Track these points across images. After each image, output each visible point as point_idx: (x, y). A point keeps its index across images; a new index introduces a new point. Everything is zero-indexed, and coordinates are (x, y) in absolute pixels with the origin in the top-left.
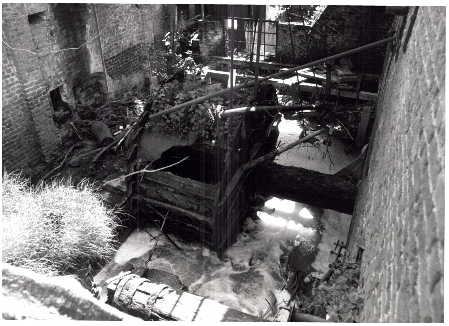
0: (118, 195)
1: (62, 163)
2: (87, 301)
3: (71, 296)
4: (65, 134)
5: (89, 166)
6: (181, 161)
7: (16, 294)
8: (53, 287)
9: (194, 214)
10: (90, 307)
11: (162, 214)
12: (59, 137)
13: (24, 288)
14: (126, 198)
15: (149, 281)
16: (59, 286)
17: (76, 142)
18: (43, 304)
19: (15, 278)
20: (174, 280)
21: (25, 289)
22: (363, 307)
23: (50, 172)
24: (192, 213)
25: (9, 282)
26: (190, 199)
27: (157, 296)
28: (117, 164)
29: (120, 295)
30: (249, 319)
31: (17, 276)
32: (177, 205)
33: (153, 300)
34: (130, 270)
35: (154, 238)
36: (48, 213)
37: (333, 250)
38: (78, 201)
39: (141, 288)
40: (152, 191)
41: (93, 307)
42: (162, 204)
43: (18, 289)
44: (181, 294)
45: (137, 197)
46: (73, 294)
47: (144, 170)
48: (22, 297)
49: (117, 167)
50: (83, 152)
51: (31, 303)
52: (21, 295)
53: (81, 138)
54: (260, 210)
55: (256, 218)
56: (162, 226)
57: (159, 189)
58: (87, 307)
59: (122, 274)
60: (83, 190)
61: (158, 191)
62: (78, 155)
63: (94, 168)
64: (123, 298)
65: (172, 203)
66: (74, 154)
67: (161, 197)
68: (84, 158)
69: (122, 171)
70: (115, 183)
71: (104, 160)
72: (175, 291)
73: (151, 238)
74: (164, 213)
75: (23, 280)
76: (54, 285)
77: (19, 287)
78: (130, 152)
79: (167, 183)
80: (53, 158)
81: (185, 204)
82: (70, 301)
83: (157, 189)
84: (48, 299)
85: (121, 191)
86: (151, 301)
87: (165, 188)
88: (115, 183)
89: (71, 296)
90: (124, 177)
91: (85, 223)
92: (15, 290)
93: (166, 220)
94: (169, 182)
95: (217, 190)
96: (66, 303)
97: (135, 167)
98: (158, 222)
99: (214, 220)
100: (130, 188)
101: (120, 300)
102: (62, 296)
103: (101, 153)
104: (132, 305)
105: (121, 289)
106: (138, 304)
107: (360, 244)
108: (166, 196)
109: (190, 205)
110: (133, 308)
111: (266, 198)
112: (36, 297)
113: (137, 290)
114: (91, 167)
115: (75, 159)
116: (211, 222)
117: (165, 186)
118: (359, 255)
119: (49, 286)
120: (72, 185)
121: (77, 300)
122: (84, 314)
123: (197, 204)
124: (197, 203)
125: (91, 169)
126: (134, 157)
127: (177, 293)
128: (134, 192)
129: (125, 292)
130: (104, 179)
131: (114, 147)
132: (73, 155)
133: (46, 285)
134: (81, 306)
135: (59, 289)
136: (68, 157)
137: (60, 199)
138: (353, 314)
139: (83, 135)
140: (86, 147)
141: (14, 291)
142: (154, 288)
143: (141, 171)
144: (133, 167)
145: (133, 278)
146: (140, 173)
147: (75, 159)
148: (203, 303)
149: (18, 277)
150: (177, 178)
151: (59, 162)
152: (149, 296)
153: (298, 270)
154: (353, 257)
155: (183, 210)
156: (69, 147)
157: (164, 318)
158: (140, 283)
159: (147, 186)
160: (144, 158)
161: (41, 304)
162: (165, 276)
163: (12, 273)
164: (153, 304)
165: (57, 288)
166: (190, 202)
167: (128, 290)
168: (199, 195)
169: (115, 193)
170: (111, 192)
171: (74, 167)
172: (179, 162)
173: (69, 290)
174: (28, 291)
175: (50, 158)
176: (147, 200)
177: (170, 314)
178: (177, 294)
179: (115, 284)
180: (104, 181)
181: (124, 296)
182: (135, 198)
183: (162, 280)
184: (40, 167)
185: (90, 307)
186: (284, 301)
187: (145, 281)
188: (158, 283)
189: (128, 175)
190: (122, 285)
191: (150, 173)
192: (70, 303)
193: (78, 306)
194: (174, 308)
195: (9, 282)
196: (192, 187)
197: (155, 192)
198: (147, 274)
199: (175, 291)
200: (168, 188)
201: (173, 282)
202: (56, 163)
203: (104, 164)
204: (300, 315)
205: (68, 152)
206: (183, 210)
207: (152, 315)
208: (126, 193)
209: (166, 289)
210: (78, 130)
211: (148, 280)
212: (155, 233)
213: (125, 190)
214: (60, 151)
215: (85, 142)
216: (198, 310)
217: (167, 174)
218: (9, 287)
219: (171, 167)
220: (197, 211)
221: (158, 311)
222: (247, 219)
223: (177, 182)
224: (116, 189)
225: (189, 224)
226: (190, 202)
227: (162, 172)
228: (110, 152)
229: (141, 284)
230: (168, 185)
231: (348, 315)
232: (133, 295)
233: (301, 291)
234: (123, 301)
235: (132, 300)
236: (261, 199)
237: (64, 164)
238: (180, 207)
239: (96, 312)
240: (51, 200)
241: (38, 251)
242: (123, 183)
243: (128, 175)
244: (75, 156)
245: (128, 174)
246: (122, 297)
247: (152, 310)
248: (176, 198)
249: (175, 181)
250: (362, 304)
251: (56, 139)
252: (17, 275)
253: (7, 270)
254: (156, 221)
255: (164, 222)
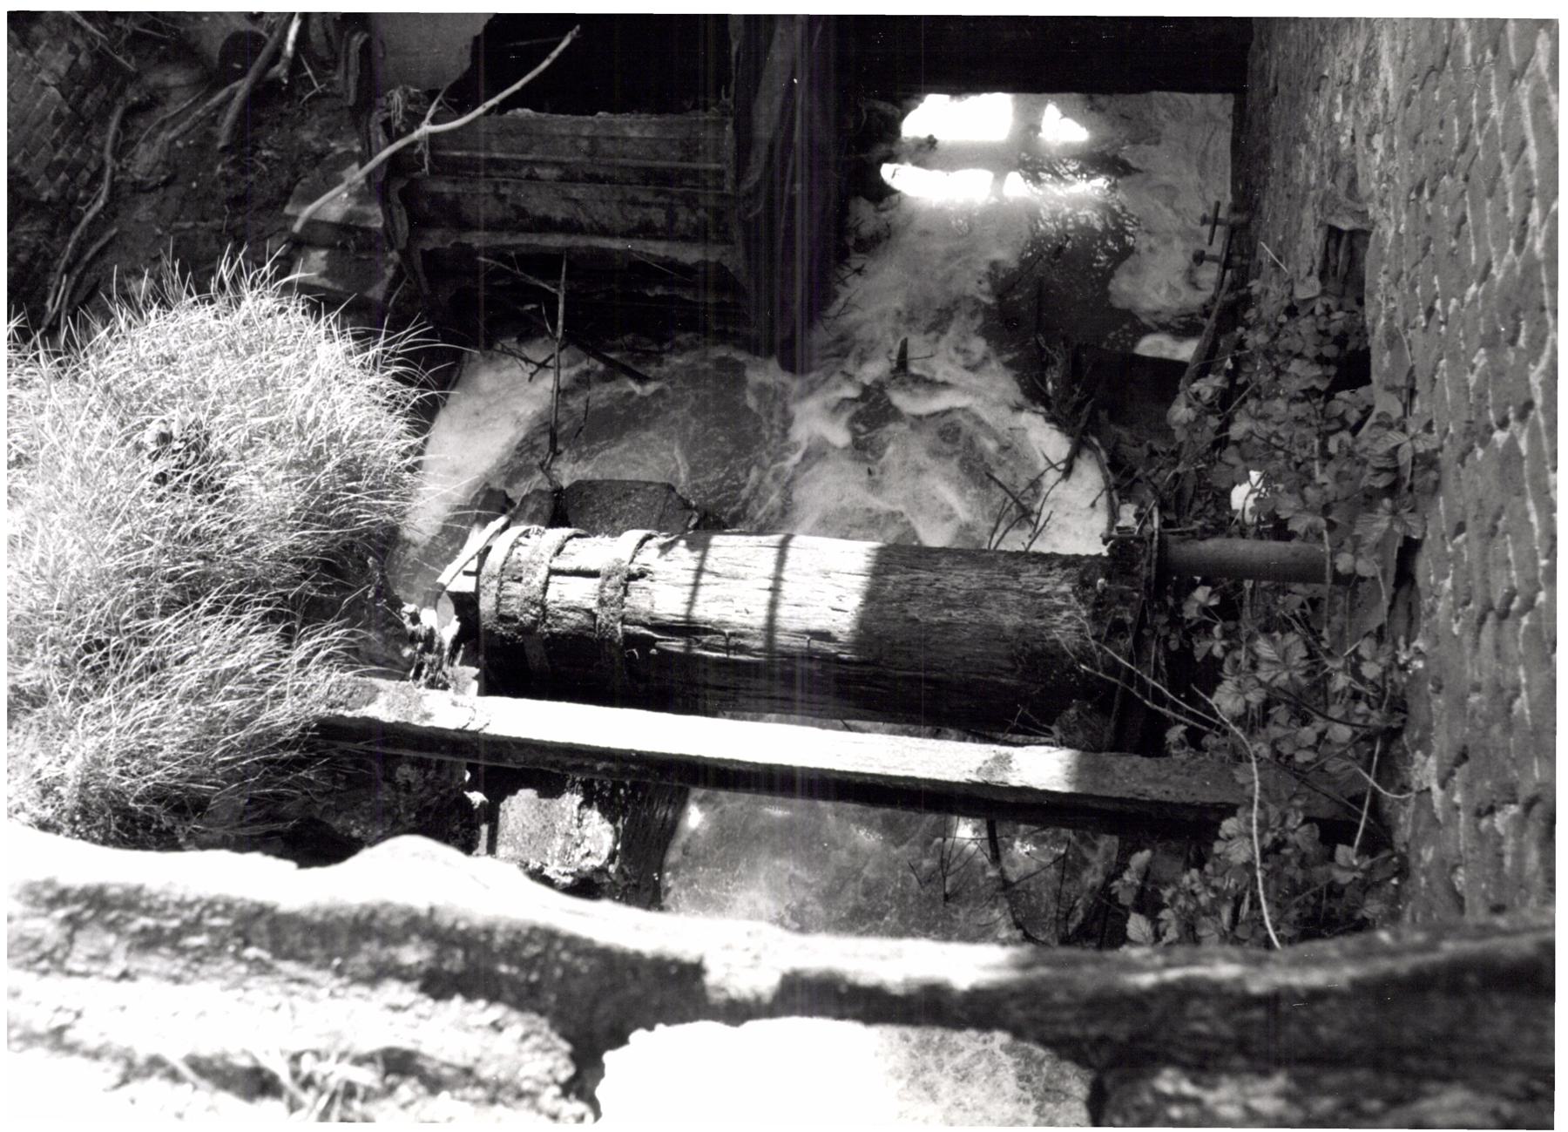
0: (360, 248)
1: (105, 188)
2: (525, 932)
3: (453, 927)
4: (62, 69)
5: (211, 168)
6: (554, 54)
7: (217, 969)
8: (365, 915)
9: (659, 249)
10: (548, 947)
11: (544, 279)
12: (44, 84)
13: (239, 941)
14: (394, 255)
15: (582, 532)
16: (385, 905)
17: (121, 91)
18: (345, 980)
19: (188, 915)
20: (661, 503)
21: (247, 944)
22: (1437, 483)
23: (74, 236)
24: (651, 244)
25: (167, 932)
26: (630, 191)
27: (625, 575)
28: (311, 129)
29: (498, 603)
30: (960, 563)
31: (191, 905)
32: (590, 226)
33: (616, 588)
34: (503, 511)
35: (542, 365)
36: (149, 437)
37: (1202, 245)
38: (241, 350)
39: (558, 564)
40: (481, 200)
41: (558, 945)
42: (535, 239)
43: (217, 950)
44: (705, 547)
45: (434, 239)
46: (456, 921)
47: (426, 128)
48: (248, 974)
49: (317, 140)
50: (163, 123)
51: (294, 987)
52: (243, 969)
53: (131, 67)
54: (891, 158)
55: (882, 193)
56: (560, 323)
57: (506, 184)
58: (532, 950)
59: (477, 538)
60: (239, 301)
61: (503, 191)
62: (151, 138)
63: (231, 172)
64: (514, 607)
65: (568, 227)
66: (132, 137)
67: (522, 212)
68: (179, 144)
69: (340, 150)
70: (334, 205)
71: (258, 131)
72: (682, 543)
73: (532, 368)
74: (551, 273)
75: (224, 914)
76: (364, 907)
77: (216, 943)
78: (346, 74)
79: (525, 152)
80: (63, 177)
81: (618, 217)
82: (454, 944)
83: (497, 185)
84: (361, 960)
85: (367, 231)
86: (609, 592)
87: (525, 171)
88: (334, 205)
89: (453, 927)
90: (356, 175)
91: (300, 424)
92: (207, 954)
93: (566, 297)
94: (532, 145)
95: (723, 130)
96: (439, 958)
97: (387, 124)
98: (539, 309)
99: (741, 253)
100: (396, 211)
101: (503, 618)
102: (415, 938)
103: (235, 105)
104: (549, 621)
105: (495, 583)
106: (571, 615)
107: (1332, 214)
108: (539, 203)
109: (637, 215)
110: (556, 630)
111: (900, 106)
112: (305, 960)
113: (553, 572)
114: (219, 169)
115: (145, 158)
116: (732, 258)
117: (522, 163)
118: (1331, 255)
119: (343, 914)
120: (190, 293)
121: (482, 938)
122: (534, 977)
123: (661, 205)
124: (661, 199)
125: (224, 176)
126: (370, 92)
127: (691, 546)
128: (420, 223)
129: (516, 589)
130: (285, 203)
131: (277, 68)
132: (134, 143)
133: (327, 913)
134: (511, 951)
135: (390, 916)
136: (118, 154)
137: (169, 360)
138: (1394, 512)
139: (134, 50)
140: (167, 95)
141: (208, 959)
142: (604, 551)
143: (416, 134)
144: (380, 129)
145: (523, 540)
146: (413, 145)
147: (145, 158)
148: (791, 553)
149: (197, 909)
150: (561, 123)
151: (92, 186)
152: (598, 581)
153: (1076, 342)
154: (1305, 268)
155: (617, 244)
156: (103, 118)
157: (671, 634)
158: (554, 551)
159: (455, 182)
160: (409, 83)
161: (336, 982)
162: (627, 495)
163: (162, 898)
164: (621, 600)
165: (383, 915)
166: (634, 202)
167: (520, 580)
168: (658, 163)
169: (344, 247)
170: (330, 246)
171: (155, 188)
172: (546, 63)
173: (432, 910)
174: (261, 946)
175: (52, 180)
176: (477, 239)
177: (688, 616)
178: (692, 550)
179: (467, 573)
180: (288, 210)
181: (513, 601)
182: (428, 246)
183: (622, 512)
184: (25, 228)
185: (548, 947)
186: (1053, 466)
187: (570, 538)
188: (616, 533)
189: (371, 165)
190: (497, 571)
191: (452, 132)
192: (459, 954)
193: (493, 955)
194: (694, 594)
195: (167, 932)
196: (627, 139)
197: (492, 202)
198: (565, 509)
199: (682, 543)
200: (538, 171)
201: (658, 509)
202: (81, 195)
203: (262, 144)
204: (1183, 548)
205: (110, 137)
206: (617, 244)
207: (627, 635)
208: (388, 234)
209: (648, 543)
210: (105, 32)
211: (579, 531)
212: (537, 352)
213: (377, 224)
214: (76, 143)
215: (153, 79)
216: (777, 579)
217: (516, 120)
218: (182, 951)
219: (524, 87)
220: (667, 233)
221: (645, 619)
222: (853, 205)
223: (563, 136)
224: (345, 228)
225: (652, 288)
226: (634, 202)
227: (494, 116)
228: (265, 94)
229: (559, 550)
230: (530, 157)
231: (1378, 520)
232: (545, 590)
233: (1103, 415)
234: (515, 619)
235: (544, 608)
236: (883, 116)
237: (114, 187)
238: (605, 232)
239: (579, 961)
240: (141, 380)
241: (173, 577)
242: (361, 196)
243: (371, 165)
244: (142, 147)
245: (371, 158)
246: (507, 606)
247: (624, 620)
248: (576, 201)
249: (553, 136)
250: (1433, 475)
251: (38, 97)
252: (190, 898)
253: (139, 889)
254: (529, 307)
255: (561, 307)
